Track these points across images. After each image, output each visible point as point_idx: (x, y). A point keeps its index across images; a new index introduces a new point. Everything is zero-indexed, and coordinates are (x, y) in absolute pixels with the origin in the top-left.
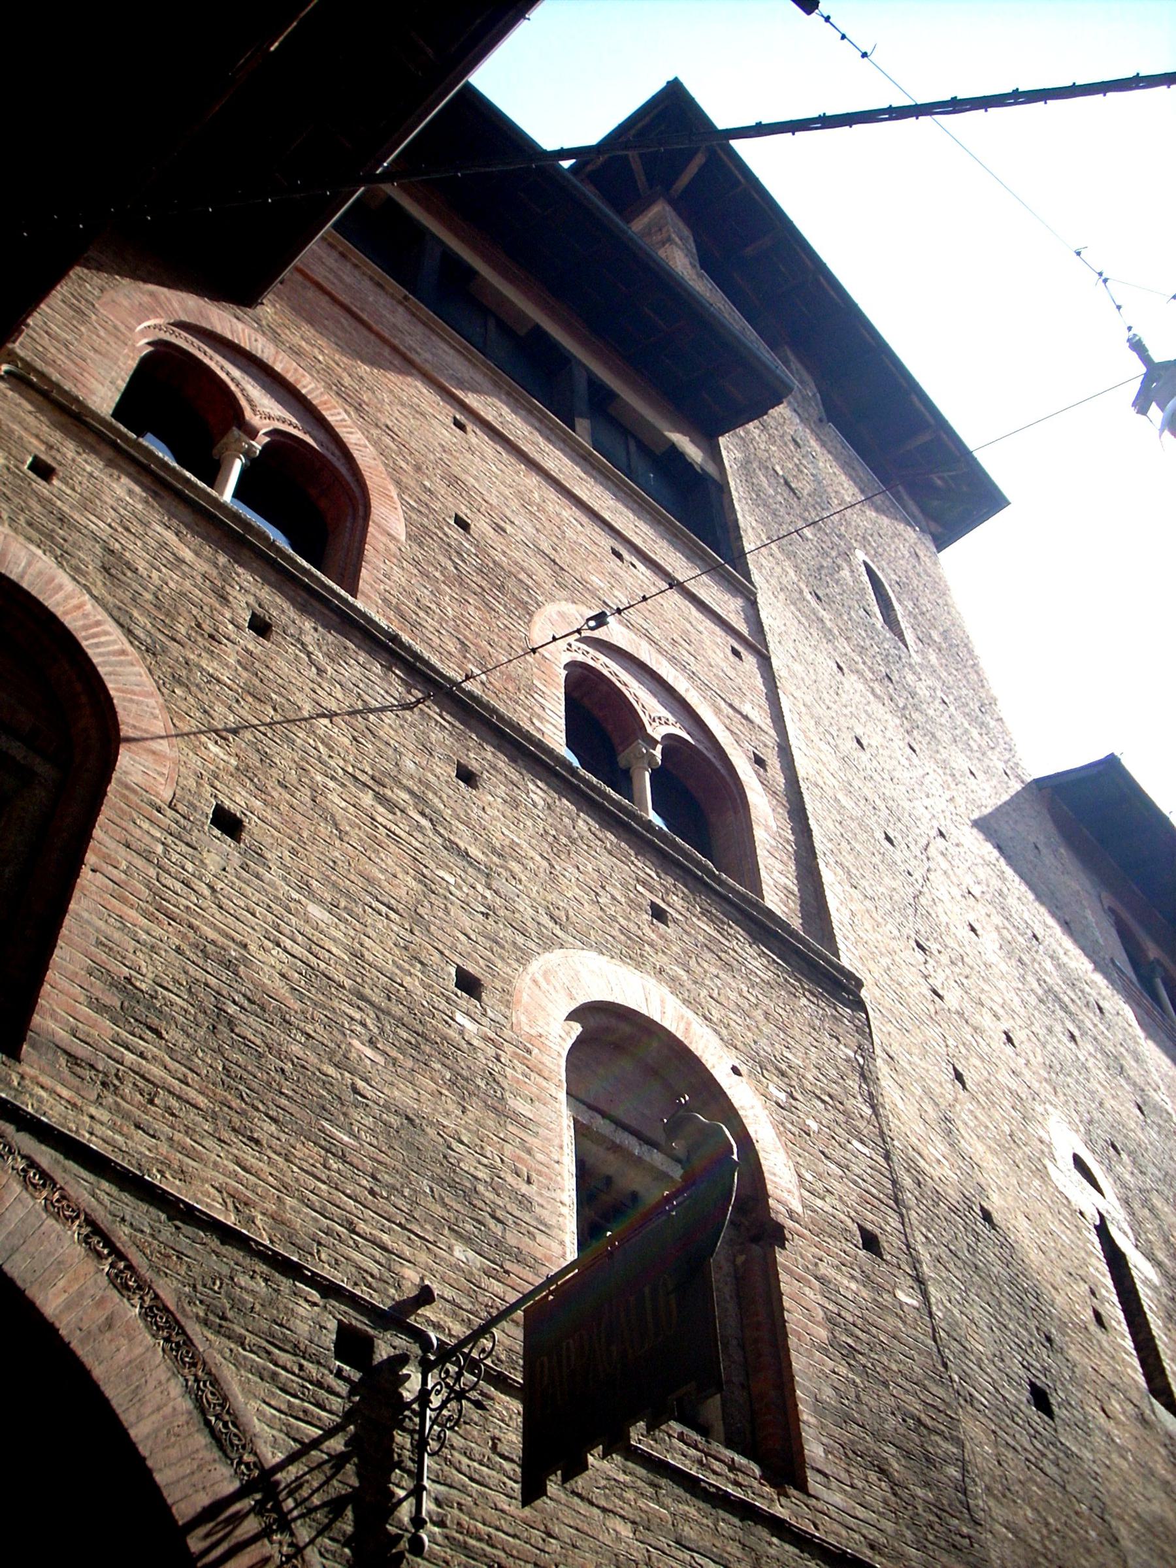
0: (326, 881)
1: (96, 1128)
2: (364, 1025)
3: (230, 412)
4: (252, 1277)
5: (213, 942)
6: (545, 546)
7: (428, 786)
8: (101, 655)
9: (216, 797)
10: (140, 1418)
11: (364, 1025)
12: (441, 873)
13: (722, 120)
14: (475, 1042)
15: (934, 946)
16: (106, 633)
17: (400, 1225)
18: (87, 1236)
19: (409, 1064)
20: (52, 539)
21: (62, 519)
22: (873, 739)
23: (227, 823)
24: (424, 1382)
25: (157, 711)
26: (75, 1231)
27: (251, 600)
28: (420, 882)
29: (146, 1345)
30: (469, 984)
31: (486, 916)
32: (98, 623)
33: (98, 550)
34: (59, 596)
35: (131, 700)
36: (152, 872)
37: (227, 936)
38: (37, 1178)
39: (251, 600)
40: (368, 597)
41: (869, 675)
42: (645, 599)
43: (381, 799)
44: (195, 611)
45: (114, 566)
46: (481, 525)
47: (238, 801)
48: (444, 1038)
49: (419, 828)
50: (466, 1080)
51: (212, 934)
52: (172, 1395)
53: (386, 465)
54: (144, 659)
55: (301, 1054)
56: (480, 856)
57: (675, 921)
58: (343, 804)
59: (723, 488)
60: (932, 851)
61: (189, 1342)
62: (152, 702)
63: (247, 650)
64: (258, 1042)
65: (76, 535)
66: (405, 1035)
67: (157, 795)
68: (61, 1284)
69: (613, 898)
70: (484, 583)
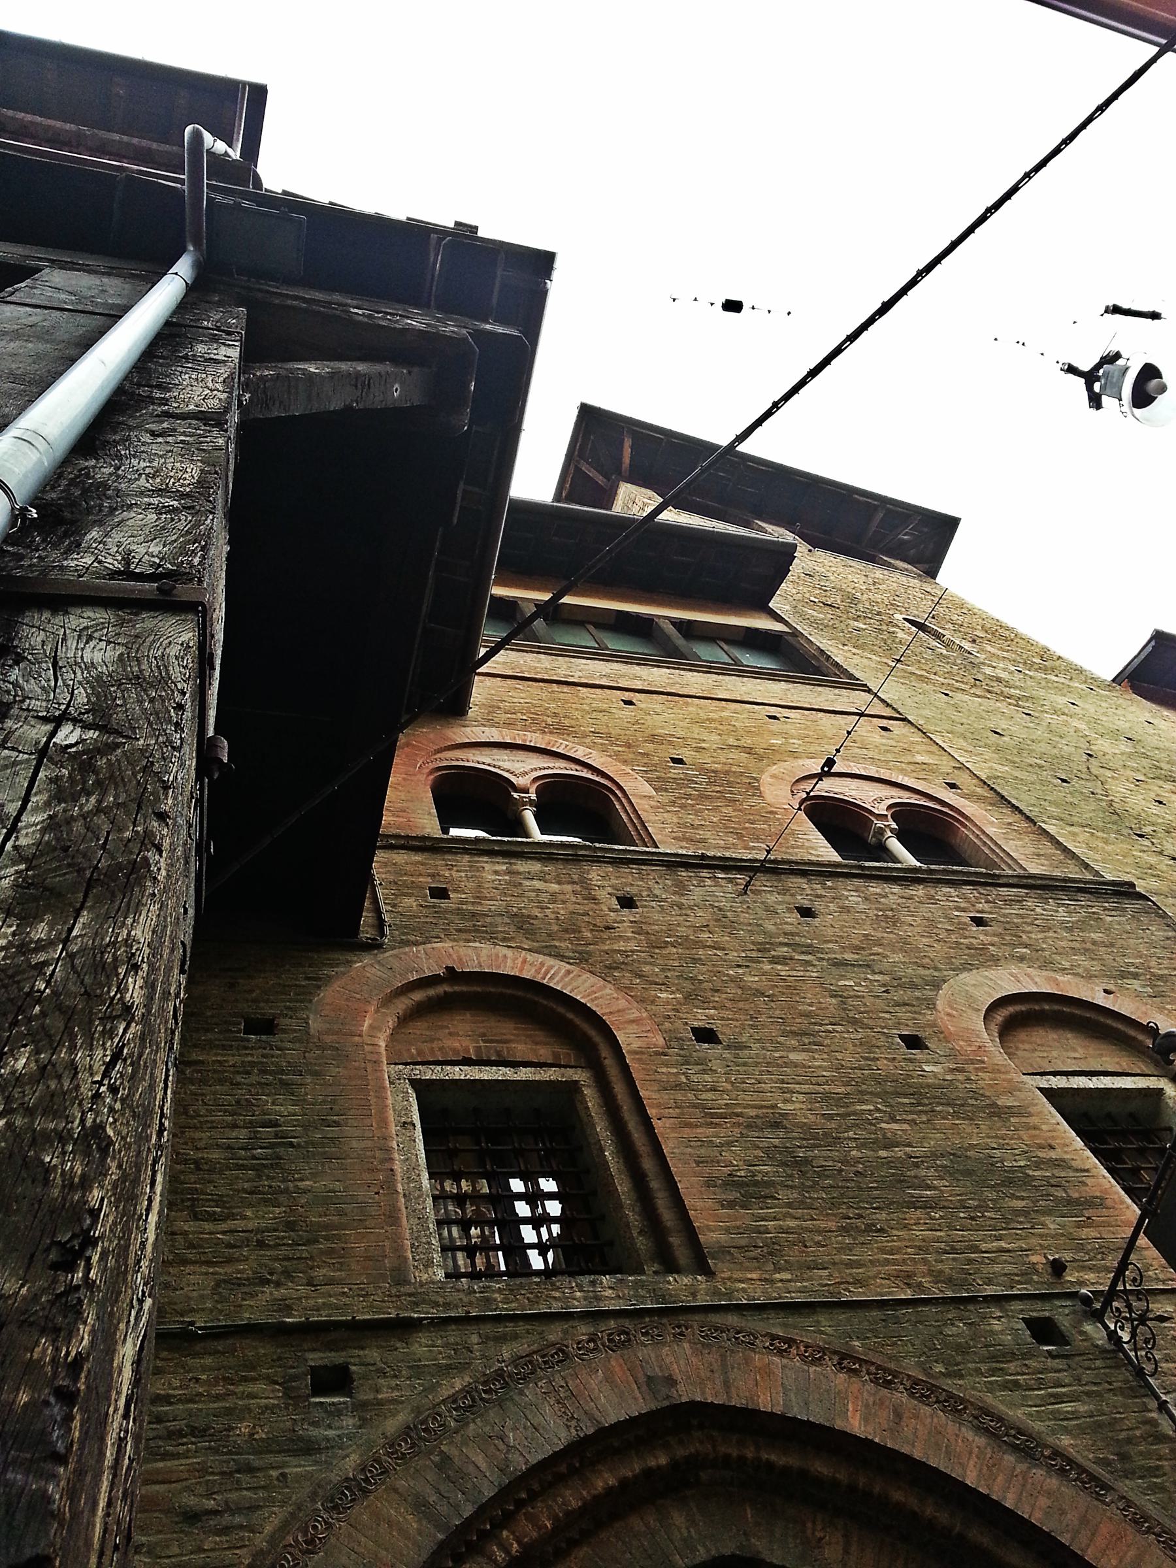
0: (785, 1034)
1: (789, 1286)
2: (878, 1110)
3: (498, 785)
4: (952, 1324)
5: (757, 1117)
6: (731, 741)
7: (792, 934)
8: (558, 982)
9: (687, 1023)
10: (964, 1467)
11: (878, 1110)
12: (841, 983)
13: (723, 439)
14: (948, 1078)
15: (1148, 829)
16: (552, 967)
17: (1004, 1229)
18: (839, 1363)
19: (924, 1118)
20: (477, 931)
21: (474, 915)
22: (1002, 725)
23: (706, 1035)
24: (1106, 1327)
25: (615, 995)
26: (830, 1362)
27: (610, 890)
28: (836, 996)
29: (931, 1416)
30: (913, 1042)
31: (887, 991)
32: (542, 964)
33: (507, 920)
34: (509, 963)
35: (596, 998)
36: (690, 1096)
37: (762, 1107)
38: (783, 1346)
39: (610, 890)
40: (665, 842)
41: (966, 687)
42: (849, 733)
43: (775, 960)
44: (586, 918)
45: (524, 925)
46: (685, 754)
47: (701, 1017)
48: (929, 1086)
49: (808, 963)
50: (963, 1105)
51: (752, 1112)
52: (971, 1439)
53: (610, 756)
54: (583, 968)
55: (860, 1155)
56: (856, 956)
57: (992, 920)
58: (756, 979)
59: (795, 633)
60: (1094, 771)
61: (951, 1396)
62: (608, 991)
63: (631, 922)
64: (830, 1163)
65: (488, 920)
66: (906, 1101)
67: (656, 1046)
68: (850, 1407)
69: (947, 930)
70: (718, 789)
